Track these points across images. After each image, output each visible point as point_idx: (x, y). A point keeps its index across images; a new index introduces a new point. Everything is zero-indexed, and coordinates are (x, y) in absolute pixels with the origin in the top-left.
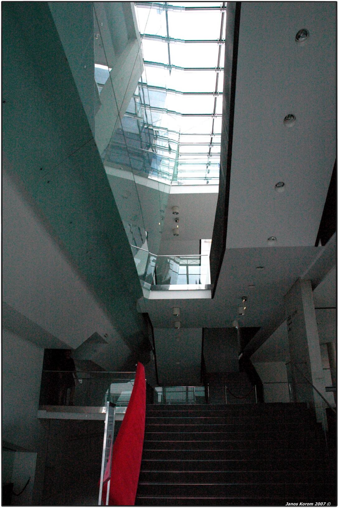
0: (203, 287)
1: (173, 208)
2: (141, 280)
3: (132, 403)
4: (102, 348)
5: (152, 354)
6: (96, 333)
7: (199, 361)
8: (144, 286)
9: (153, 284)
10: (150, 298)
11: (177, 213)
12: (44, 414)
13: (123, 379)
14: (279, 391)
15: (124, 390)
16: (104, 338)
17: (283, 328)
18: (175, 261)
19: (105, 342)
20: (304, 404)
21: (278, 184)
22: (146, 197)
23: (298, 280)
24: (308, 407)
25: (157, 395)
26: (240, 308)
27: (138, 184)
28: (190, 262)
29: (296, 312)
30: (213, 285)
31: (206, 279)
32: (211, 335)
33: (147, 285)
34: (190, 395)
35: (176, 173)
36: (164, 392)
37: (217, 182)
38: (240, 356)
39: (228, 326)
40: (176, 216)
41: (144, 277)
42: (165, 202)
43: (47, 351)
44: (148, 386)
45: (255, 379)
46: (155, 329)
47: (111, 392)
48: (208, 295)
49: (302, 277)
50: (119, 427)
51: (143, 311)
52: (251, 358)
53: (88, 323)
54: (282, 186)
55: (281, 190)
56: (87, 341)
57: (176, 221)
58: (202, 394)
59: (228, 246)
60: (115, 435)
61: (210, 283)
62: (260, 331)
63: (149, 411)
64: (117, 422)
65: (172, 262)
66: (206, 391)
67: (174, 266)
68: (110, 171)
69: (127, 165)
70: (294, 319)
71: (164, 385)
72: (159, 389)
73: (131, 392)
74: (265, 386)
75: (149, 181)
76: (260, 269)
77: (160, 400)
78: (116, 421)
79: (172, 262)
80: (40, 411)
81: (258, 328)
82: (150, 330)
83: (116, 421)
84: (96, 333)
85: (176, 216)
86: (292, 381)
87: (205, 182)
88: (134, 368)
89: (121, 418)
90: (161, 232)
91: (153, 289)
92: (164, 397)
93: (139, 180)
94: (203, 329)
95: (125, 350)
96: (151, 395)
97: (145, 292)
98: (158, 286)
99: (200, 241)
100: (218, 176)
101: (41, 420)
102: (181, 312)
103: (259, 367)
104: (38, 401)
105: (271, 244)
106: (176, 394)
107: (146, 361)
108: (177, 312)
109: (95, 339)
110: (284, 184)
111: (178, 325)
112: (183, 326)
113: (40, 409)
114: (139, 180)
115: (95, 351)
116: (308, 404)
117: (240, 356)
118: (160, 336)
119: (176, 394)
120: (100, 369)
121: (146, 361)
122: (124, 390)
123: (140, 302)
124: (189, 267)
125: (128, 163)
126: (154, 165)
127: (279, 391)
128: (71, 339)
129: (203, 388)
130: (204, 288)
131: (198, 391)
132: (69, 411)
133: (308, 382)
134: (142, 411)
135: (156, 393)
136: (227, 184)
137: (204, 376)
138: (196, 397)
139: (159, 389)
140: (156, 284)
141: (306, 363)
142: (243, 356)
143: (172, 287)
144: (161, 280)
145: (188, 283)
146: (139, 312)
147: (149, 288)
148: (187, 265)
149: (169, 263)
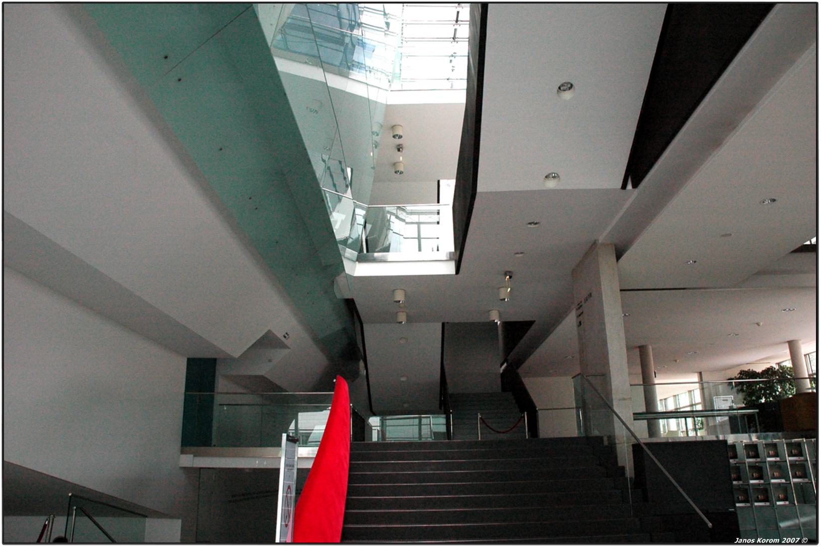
0: (443, 255)
1: (393, 127)
2: (340, 246)
3: (325, 444)
4: (279, 355)
5: (362, 364)
6: (269, 332)
7: (437, 375)
8: (347, 255)
9: (361, 251)
10: (356, 274)
11: (400, 137)
12: (188, 460)
13: (314, 404)
14: (561, 421)
15: (314, 422)
16: (283, 339)
17: (570, 320)
18: (397, 217)
19: (284, 346)
20: (600, 439)
21: (562, 85)
22: (333, 104)
23: (595, 243)
24: (606, 443)
25: (371, 430)
26: (502, 290)
27: (333, 88)
28: (423, 218)
29: (590, 295)
30: (458, 253)
31: (449, 245)
32: (458, 335)
33: (350, 253)
34: (425, 430)
35: (397, 71)
36: (383, 425)
37: (464, 84)
38: (503, 367)
39: (483, 319)
40: (398, 141)
41: (345, 242)
42: (379, 118)
43: (188, 359)
44: (355, 414)
45: (526, 404)
46: (364, 325)
47: (299, 426)
48: (449, 269)
49: (601, 239)
50: (305, 480)
51: (348, 296)
52: (520, 371)
53: (258, 316)
54: (570, 88)
55: (567, 95)
56: (254, 346)
57: (399, 150)
58: (443, 429)
59: (480, 188)
60: (298, 492)
61: (453, 250)
62: (533, 327)
63: (353, 455)
64: (300, 471)
65: (393, 218)
66: (448, 425)
67: (396, 225)
68: (283, 65)
69: (314, 56)
70: (581, 302)
71: (383, 413)
72: (374, 421)
73: (324, 427)
74: (540, 414)
75: (350, 83)
76: (533, 226)
77: (375, 438)
78: (298, 469)
79: (393, 218)
80: (183, 456)
81: (530, 323)
82: (357, 324)
83: (298, 469)
84: (269, 332)
85: (398, 141)
86: (582, 405)
87: (447, 85)
88: (332, 387)
89: (309, 465)
90: (373, 168)
91: (361, 259)
92: (383, 433)
93: (335, 82)
94: (443, 324)
95: (315, 360)
96: (361, 429)
97: (347, 265)
98: (370, 254)
99: (439, 182)
100: (466, 77)
101: (186, 469)
102: (406, 295)
103: (532, 384)
104: (180, 440)
105: (551, 184)
106: (402, 429)
107: (352, 376)
108: (400, 296)
109: (268, 341)
110: (572, 85)
111: (402, 317)
112: (410, 319)
113: (182, 452)
114: (335, 82)
115: (270, 361)
116: (605, 439)
117: (503, 367)
118: (375, 338)
119: (402, 429)
120: (280, 389)
121: (352, 376)
122: (314, 422)
123: (340, 279)
124: (422, 226)
125: (317, 54)
126: (358, 56)
127: (561, 421)
128: (230, 340)
129: (442, 420)
130: (445, 258)
131: (435, 424)
132: (223, 456)
133: (607, 406)
134: (345, 453)
135: (370, 428)
136: (478, 86)
137: (445, 399)
138: (435, 433)
139: (374, 421)
140: (367, 251)
141: (604, 376)
142: (507, 367)
143: (390, 256)
144: (372, 246)
145: (420, 250)
146: (339, 296)
147: (355, 259)
148: (419, 224)
149: (389, 221)
